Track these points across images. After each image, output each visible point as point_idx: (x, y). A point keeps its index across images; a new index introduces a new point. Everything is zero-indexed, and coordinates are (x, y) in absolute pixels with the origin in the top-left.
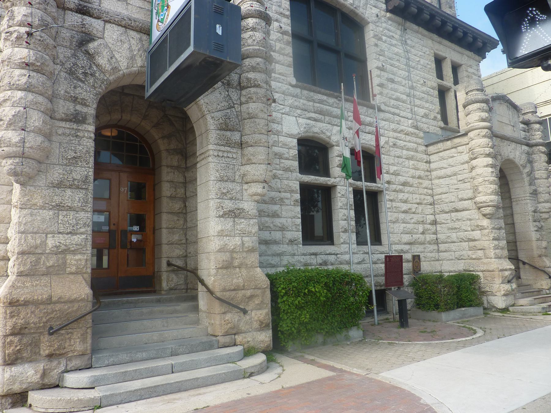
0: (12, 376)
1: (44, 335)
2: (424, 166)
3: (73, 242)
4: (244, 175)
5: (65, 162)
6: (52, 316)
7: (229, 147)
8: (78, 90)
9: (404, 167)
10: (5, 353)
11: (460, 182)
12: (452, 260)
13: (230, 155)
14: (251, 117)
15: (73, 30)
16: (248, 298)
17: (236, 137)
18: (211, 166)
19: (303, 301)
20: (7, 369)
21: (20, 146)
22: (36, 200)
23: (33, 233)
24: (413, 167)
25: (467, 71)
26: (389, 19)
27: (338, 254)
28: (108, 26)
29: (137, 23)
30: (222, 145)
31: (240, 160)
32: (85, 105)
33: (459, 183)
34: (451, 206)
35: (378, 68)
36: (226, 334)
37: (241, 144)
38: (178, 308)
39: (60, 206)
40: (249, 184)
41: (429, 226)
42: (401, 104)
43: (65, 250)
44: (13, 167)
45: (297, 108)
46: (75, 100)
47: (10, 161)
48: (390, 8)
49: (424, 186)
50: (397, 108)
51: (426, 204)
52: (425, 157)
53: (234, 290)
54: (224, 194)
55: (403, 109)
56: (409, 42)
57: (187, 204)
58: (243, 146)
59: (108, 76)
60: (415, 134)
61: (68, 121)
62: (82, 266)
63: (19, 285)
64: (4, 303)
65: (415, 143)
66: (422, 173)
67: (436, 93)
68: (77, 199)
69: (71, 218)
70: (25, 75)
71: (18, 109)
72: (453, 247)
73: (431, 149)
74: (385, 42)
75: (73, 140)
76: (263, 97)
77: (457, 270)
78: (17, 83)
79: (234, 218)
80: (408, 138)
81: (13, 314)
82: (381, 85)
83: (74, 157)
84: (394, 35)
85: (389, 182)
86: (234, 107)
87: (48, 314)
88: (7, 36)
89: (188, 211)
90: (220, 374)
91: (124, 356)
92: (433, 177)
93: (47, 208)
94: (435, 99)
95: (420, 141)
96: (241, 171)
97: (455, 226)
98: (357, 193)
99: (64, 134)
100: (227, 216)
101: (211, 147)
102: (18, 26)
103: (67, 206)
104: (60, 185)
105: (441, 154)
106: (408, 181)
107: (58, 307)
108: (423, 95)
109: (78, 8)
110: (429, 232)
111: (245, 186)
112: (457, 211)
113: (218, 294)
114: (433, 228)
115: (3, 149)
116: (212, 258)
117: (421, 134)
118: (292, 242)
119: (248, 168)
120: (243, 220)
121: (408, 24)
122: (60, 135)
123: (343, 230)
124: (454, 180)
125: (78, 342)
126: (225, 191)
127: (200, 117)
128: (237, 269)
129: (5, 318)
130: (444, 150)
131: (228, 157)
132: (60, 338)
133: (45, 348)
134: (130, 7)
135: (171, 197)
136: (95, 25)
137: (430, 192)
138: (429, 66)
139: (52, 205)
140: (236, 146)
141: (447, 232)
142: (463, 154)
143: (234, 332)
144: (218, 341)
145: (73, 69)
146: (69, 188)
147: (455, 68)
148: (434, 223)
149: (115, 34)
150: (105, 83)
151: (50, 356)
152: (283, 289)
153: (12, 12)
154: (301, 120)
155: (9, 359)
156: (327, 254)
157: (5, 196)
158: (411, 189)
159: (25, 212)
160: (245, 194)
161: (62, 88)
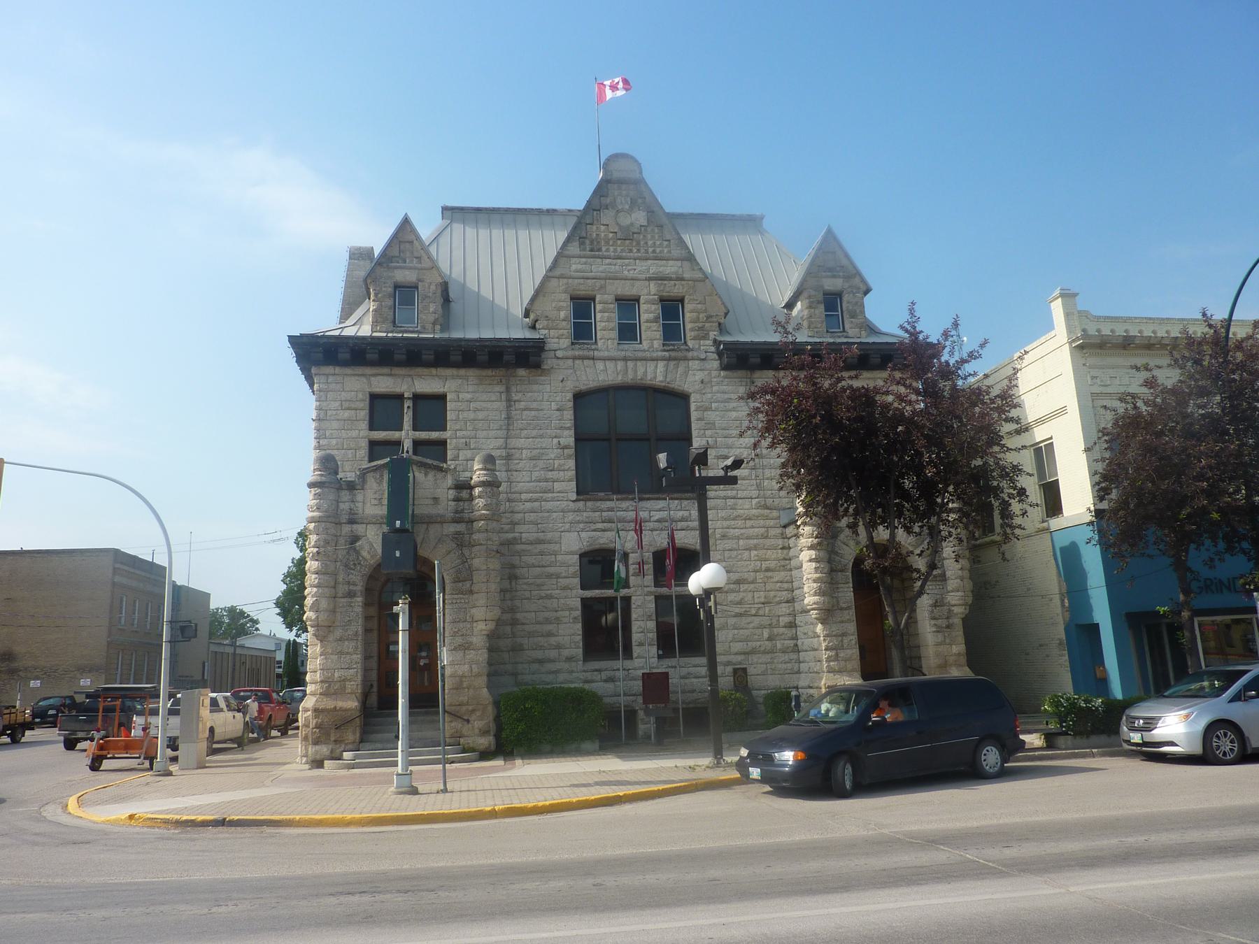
9: (741, 560)
26: (725, 377)
45: (579, 522)
46: (349, 583)
49: (776, 579)
51: (779, 603)
52: (780, 542)
80: (749, 523)
91: (379, 745)
104: (341, 639)
114: (789, 632)
118: (569, 659)
125: (352, 735)
136: (359, 529)
137: (785, 586)
154: (583, 535)
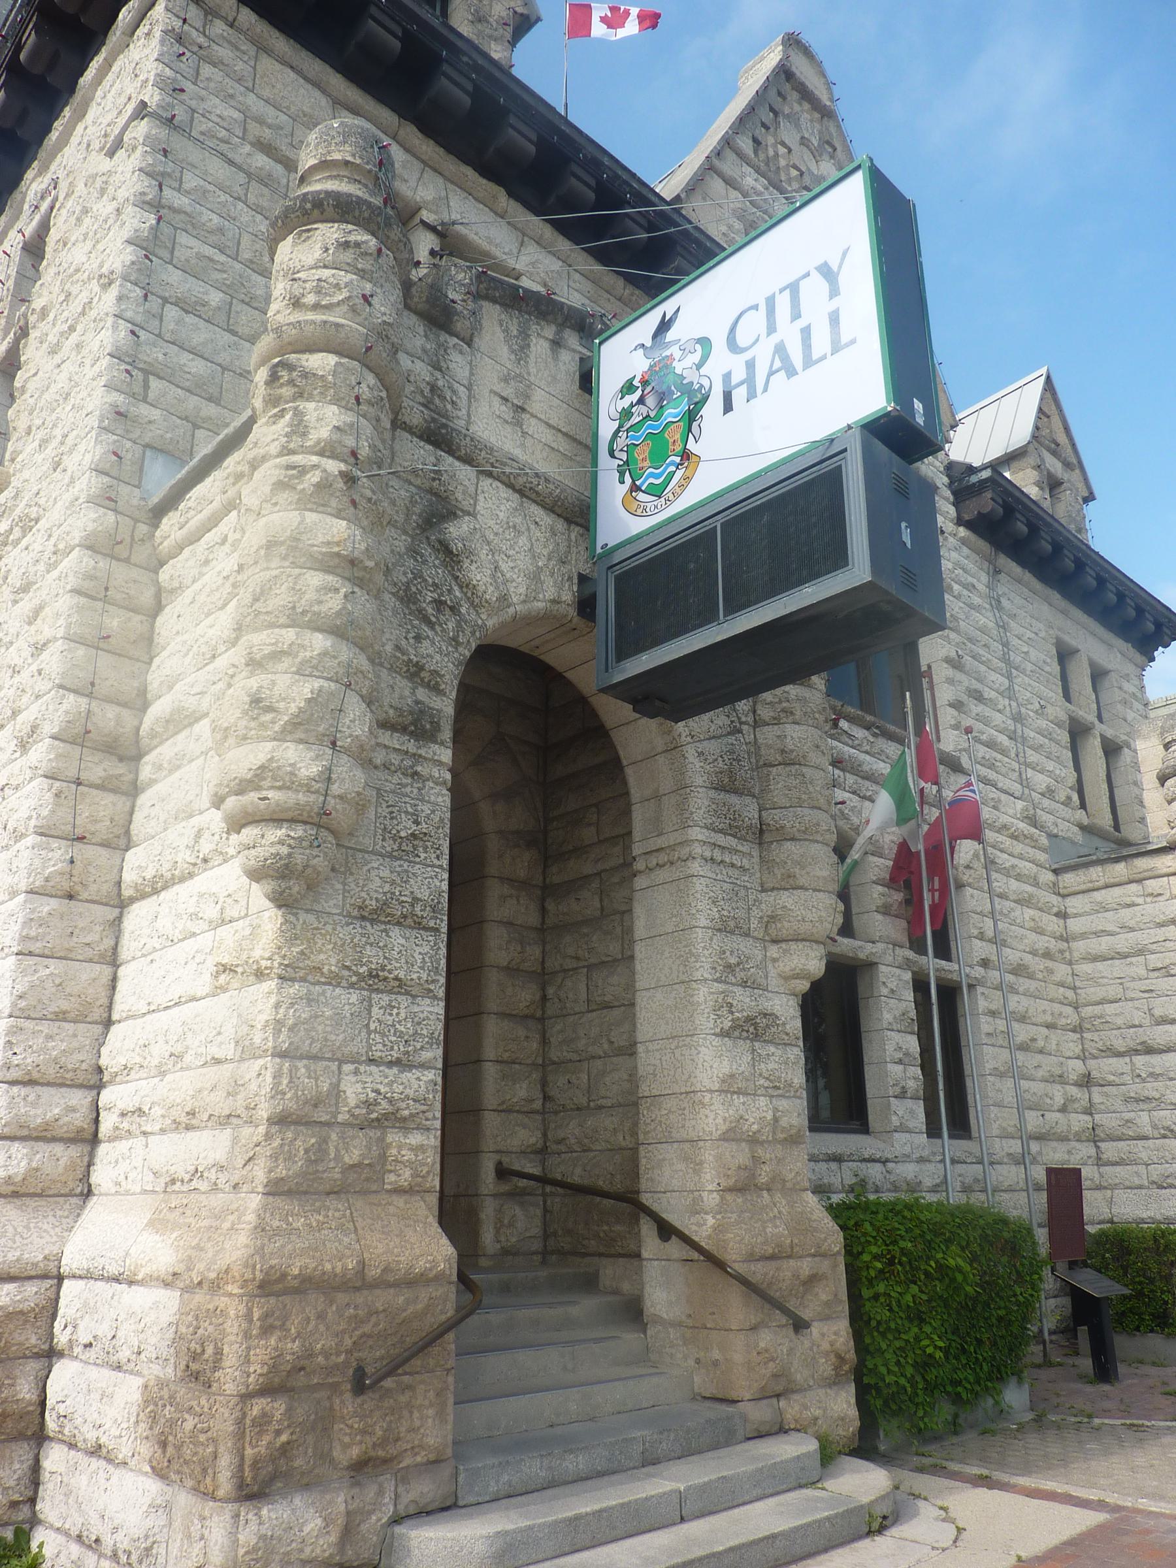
0: (263, 1538)
1: (341, 1394)
2: (1052, 924)
3: (407, 1091)
4: (773, 918)
5: (389, 845)
6: (367, 1329)
7: (735, 837)
8: (426, 648)
10: (242, 1458)
11: (1156, 974)
12: (1140, 1187)
13: (736, 859)
14: (790, 760)
15: (410, 483)
16: (804, 1283)
17: (749, 810)
18: (698, 887)
19: (925, 1297)
20: (247, 1512)
21: (317, 792)
22: (322, 956)
23: (309, 1058)
24: (1032, 924)
25: (1120, 688)
26: (963, 541)
27: (887, 1161)
28: (486, 483)
29: (551, 486)
30: (721, 831)
31: (758, 875)
32: (436, 689)
33: (1152, 974)
34: (1131, 1038)
35: (948, 660)
36: (763, 1396)
37: (761, 831)
38: (575, 1311)
39: (377, 976)
40: (784, 945)
41: (1073, 1091)
42: (999, 757)
43: (386, 1116)
44: (285, 850)
47: (275, 834)
48: (967, 517)
49: (1057, 977)
50: (991, 767)
52: (1055, 899)
53: (772, 1257)
54: (729, 968)
55: (1004, 770)
56: (1005, 603)
57: (551, 991)
58: (767, 837)
59: (484, 617)
60: (1031, 837)
61: (396, 730)
62: (425, 1169)
63: (276, 1223)
64: (245, 1283)
65: (1032, 862)
66: (1053, 945)
67: (1065, 737)
68: (418, 958)
69: (403, 1015)
70: (337, 590)
71: (317, 684)
72: (1142, 1150)
73: (1070, 880)
74: (958, 597)
75: (406, 786)
76: (820, 713)
77: (1159, 1217)
78: (316, 608)
79: (752, 1040)
80: (1019, 848)
81: (270, 1321)
82: (957, 705)
83: (413, 835)
84: (974, 581)
85: (985, 963)
86: (740, 731)
87: (359, 1321)
88: (292, 477)
89: (549, 1012)
90: (819, 1521)
91: (533, 1468)
92: (1076, 955)
93: (344, 983)
94: (1065, 751)
95: (1042, 857)
96: (763, 906)
97: (1146, 1093)
98: (920, 985)
99: (386, 766)
100: (737, 1033)
101: (697, 833)
102: (317, 454)
103: (396, 979)
105: (1098, 896)
106: (1025, 962)
107: (381, 1299)
108: (1041, 740)
109: (428, 428)
110: (1076, 1106)
111: (773, 951)
112: (1150, 1050)
113: (740, 1268)
115: (264, 794)
116: (708, 1155)
117: (1044, 841)
119: (786, 899)
120: (772, 1049)
121: (1004, 561)
122: (376, 767)
123: (898, 1090)
124: (1137, 967)
126: (733, 961)
127: (660, 750)
128: (765, 1193)
129: (247, 1335)
130: (1107, 887)
131: (733, 865)
132: (386, 1404)
133: (347, 1439)
134: (529, 442)
135: (511, 970)
138: (1047, 669)
139: (357, 974)
140: (750, 837)
141: (1122, 1108)
142: (1160, 898)
143: (779, 1388)
144: (744, 1418)
145: (414, 589)
146: (399, 924)
147: (1098, 676)
148: (1086, 1081)
149: (503, 508)
150: (478, 634)
151: (361, 1468)
152: (876, 1257)
153: (298, 414)
155: (254, 1479)
156: (865, 1160)
157: (97, 937)
158: (1032, 985)
159: (295, 989)
160: (773, 973)
161: (387, 636)
